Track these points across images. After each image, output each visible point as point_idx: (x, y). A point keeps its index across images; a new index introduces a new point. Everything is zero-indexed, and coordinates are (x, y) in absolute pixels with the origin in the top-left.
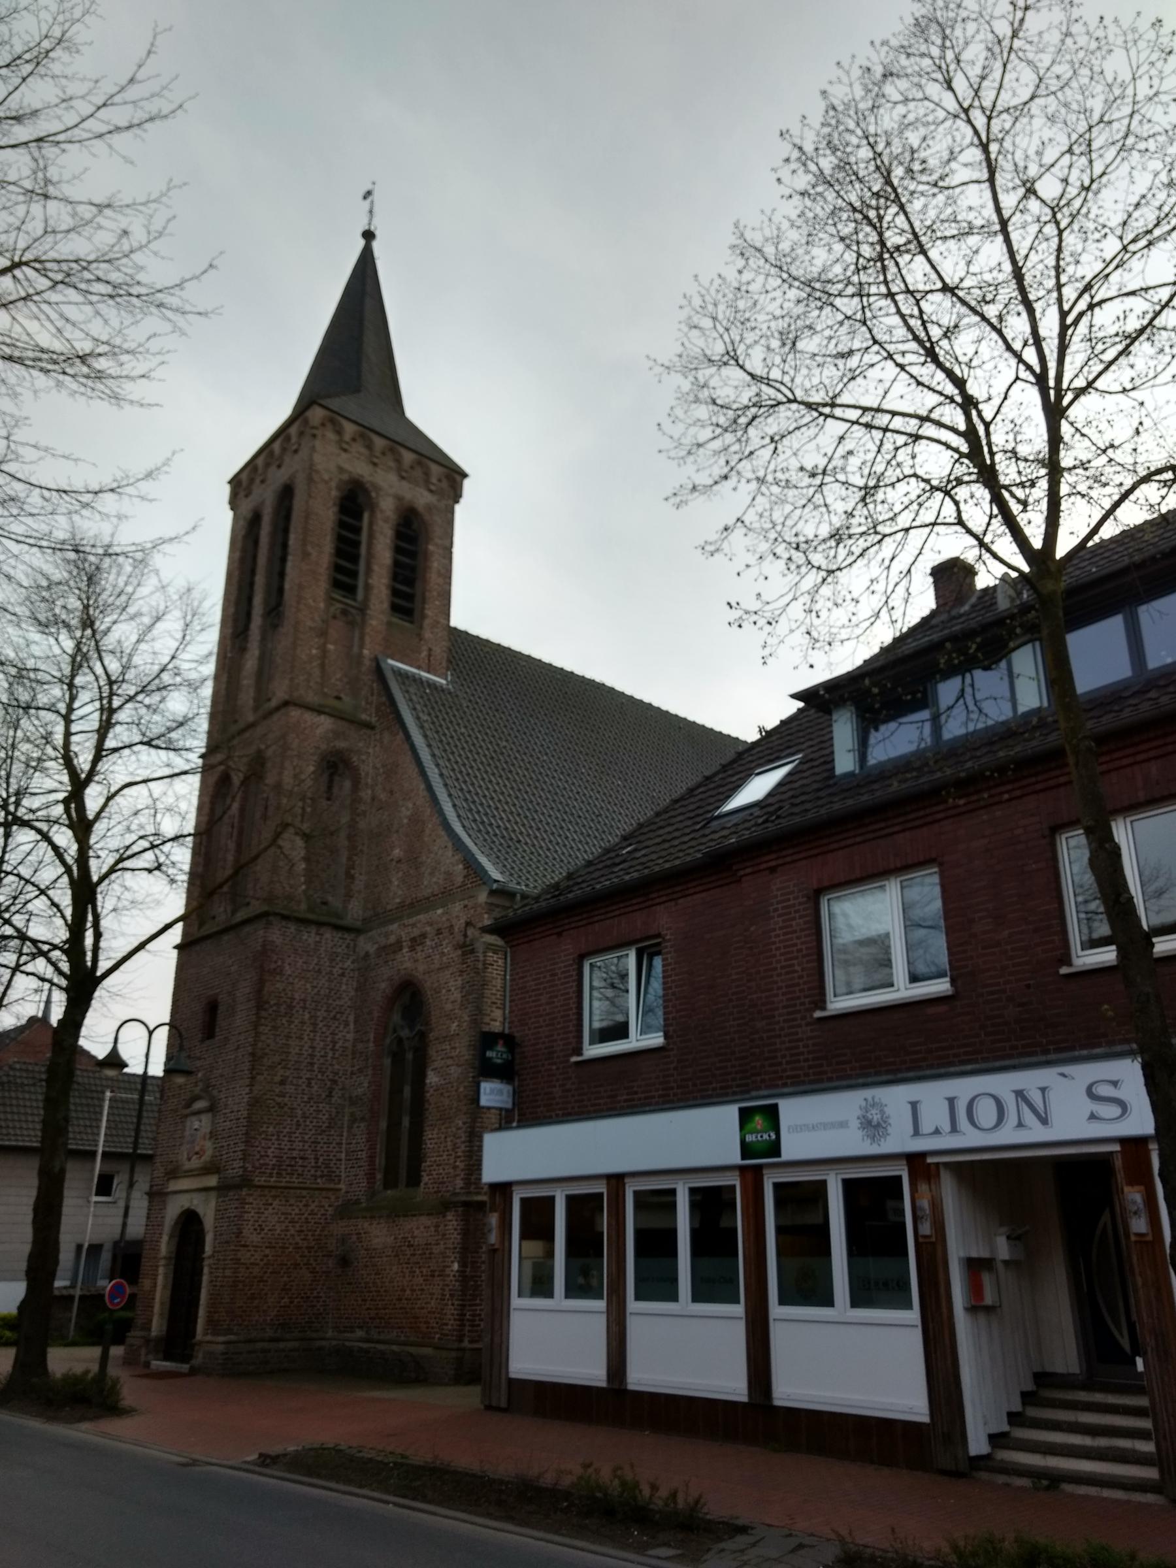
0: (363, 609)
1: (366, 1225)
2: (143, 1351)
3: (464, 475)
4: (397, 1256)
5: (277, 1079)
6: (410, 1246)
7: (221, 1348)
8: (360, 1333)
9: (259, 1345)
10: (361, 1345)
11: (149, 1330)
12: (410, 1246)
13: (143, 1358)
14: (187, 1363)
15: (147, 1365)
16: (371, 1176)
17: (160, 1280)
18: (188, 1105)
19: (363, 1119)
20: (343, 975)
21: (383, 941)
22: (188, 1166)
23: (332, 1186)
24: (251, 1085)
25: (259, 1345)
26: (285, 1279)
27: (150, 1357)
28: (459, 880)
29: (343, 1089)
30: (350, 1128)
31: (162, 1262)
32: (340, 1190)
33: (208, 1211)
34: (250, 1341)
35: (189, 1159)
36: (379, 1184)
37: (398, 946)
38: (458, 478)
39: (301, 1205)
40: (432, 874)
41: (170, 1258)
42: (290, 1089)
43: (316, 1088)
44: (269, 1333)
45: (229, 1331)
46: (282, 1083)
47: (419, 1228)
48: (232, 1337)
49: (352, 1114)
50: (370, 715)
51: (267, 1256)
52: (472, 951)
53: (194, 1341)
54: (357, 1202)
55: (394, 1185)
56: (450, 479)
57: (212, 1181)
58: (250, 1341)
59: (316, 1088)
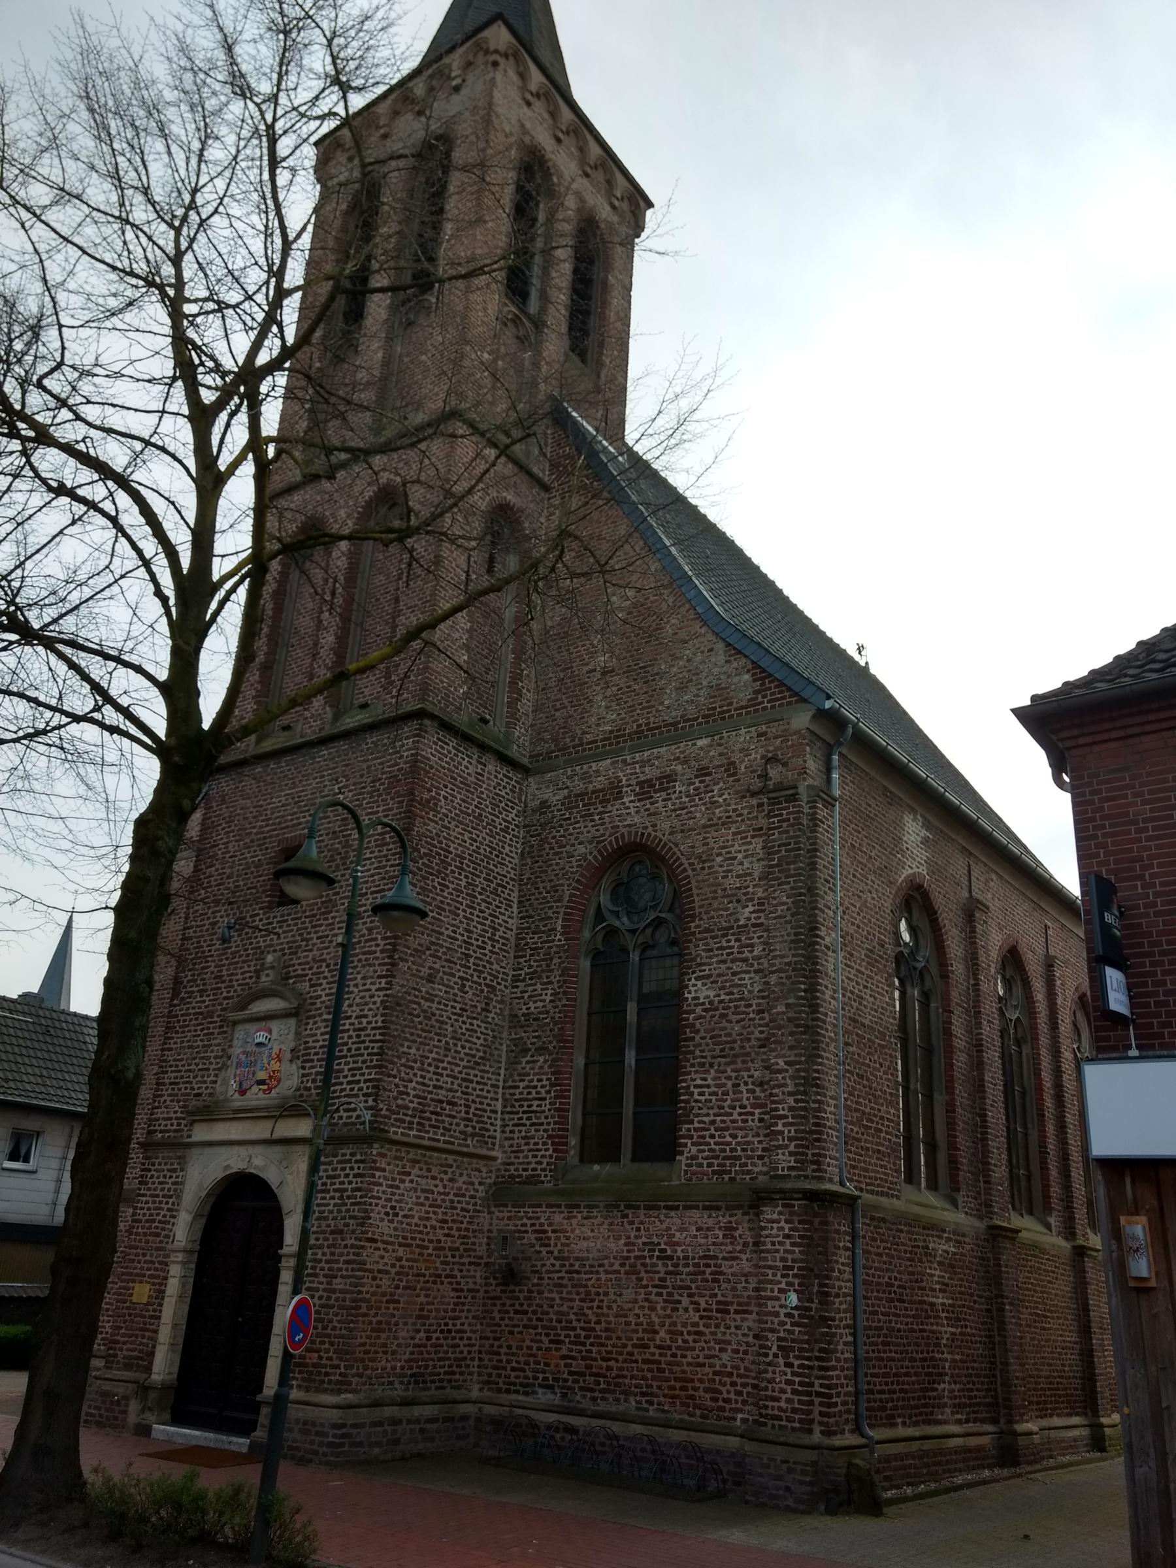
0: (538, 324)
1: (558, 1218)
2: (134, 1406)
3: (650, 205)
4: (633, 1271)
5: (425, 971)
6: (664, 1257)
7: (334, 1415)
8: (544, 1397)
9: (389, 1411)
10: (1076, 1458)
11: (148, 1369)
12: (664, 1257)
13: (132, 1418)
14: (245, 1433)
15: (144, 1431)
16: (558, 1141)
17: (173, 1287)
18: (243, 1006)
19: (542, 1050)
20: (505, 830)
21: (578, 786)
22: (238, 1102)
23: (483, 1152)
24: (390, 975)
25: (389, 1411)
26: (422, 1299)
27: (150, 1417)
28: (744, 696)
29: (501, 1002)
30: (512, 1063)
31: (180, 1257)
32: (495, 1159)
33: (289, 1181)
34: (376, 1404)
35: (243, 1092)
36: (573, 1155)
37: (614, 791)
38: (642, 204)
39: (446, 1177)
40: (682, 688)
41: (191, 1252)
42: (439, 990)
43: (470, 995)
44: (399, 1391)
45: (342, 1386)
46: (430, 979)
47: (688, 1232)
48: (349, 1397)
49: (516, 1042)
50: (543, 471)
51: (400, 1259)
52: (793, 798)
53: (259, 1398)
54: (532, 1180)
55: (611, 1154)
56: (637, 202)
57: (302, 1128)
58: (376, 1404)
59: (470, 995)
